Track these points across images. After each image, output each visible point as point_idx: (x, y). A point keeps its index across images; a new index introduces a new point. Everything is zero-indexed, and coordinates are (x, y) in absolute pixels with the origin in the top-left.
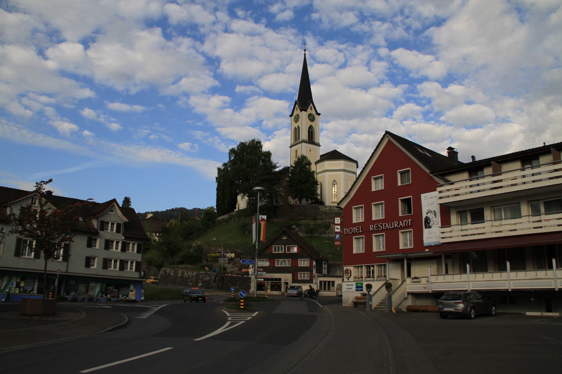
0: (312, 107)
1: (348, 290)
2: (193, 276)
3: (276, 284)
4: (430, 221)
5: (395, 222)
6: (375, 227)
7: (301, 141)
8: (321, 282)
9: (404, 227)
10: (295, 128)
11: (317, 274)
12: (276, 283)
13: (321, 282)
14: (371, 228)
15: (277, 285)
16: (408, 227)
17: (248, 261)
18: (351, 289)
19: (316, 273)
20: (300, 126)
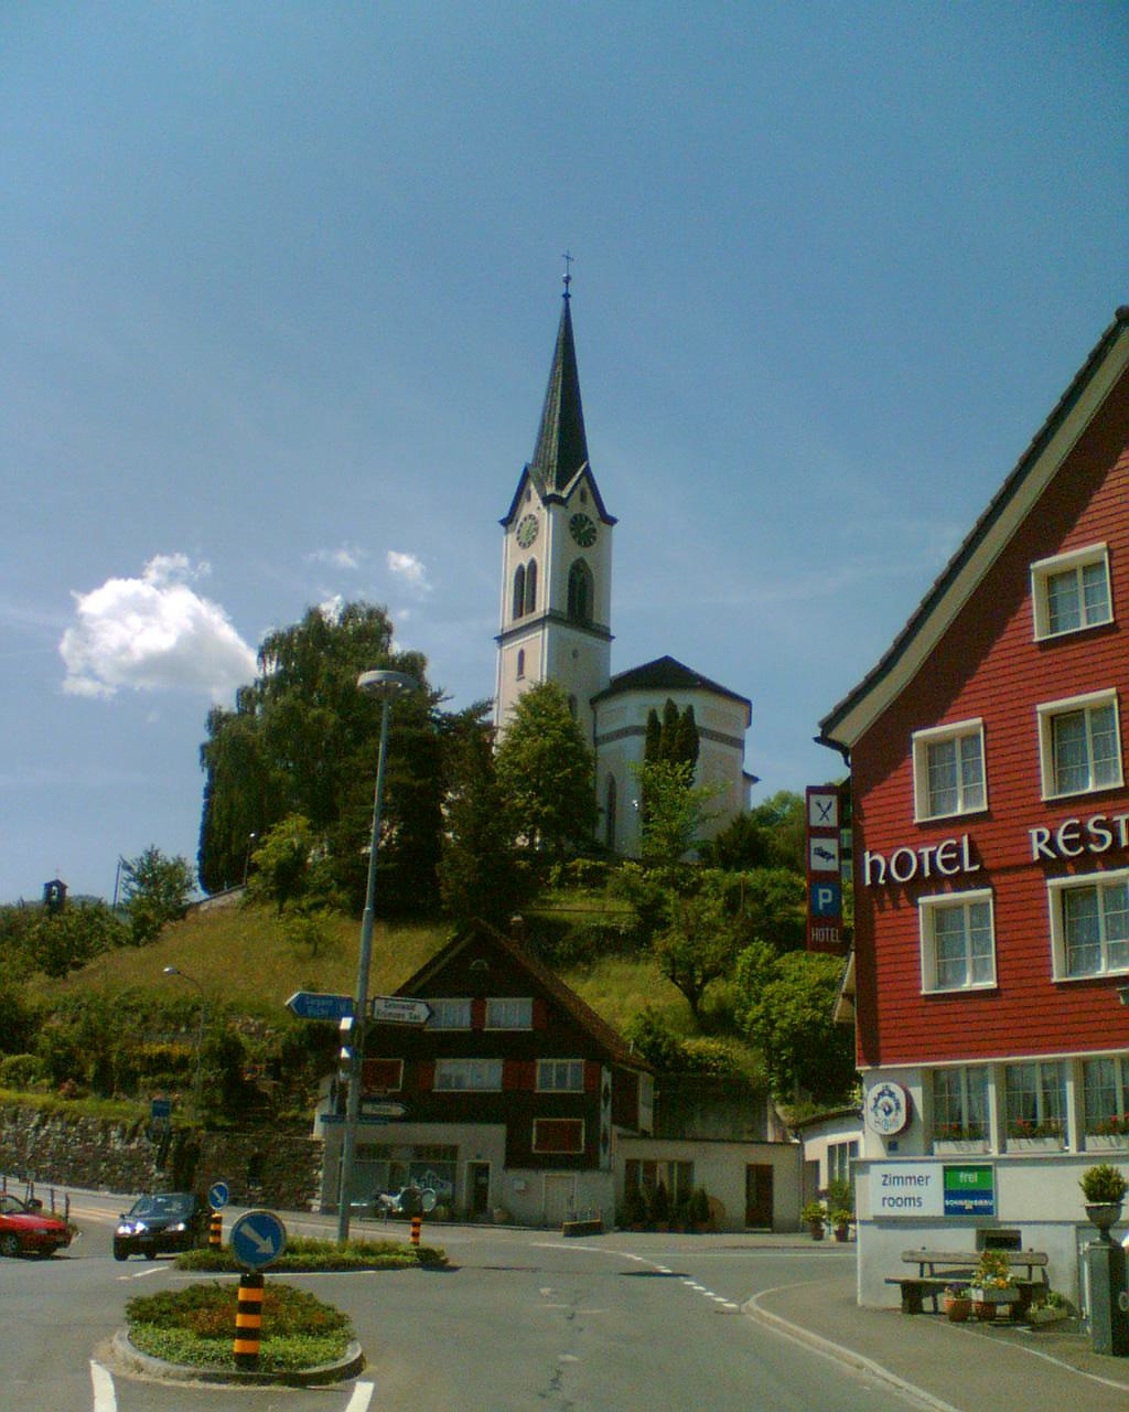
0: (588, 491)
6: (1060, 838)
7: (542, 616)
8: (631, 1165)
10: (521, 568)
11: (617, 1129)
13: (631, 1165)
14: (1037, 847)
18: (918, 1201)
19: (614, 1121)
20: (538, 562)
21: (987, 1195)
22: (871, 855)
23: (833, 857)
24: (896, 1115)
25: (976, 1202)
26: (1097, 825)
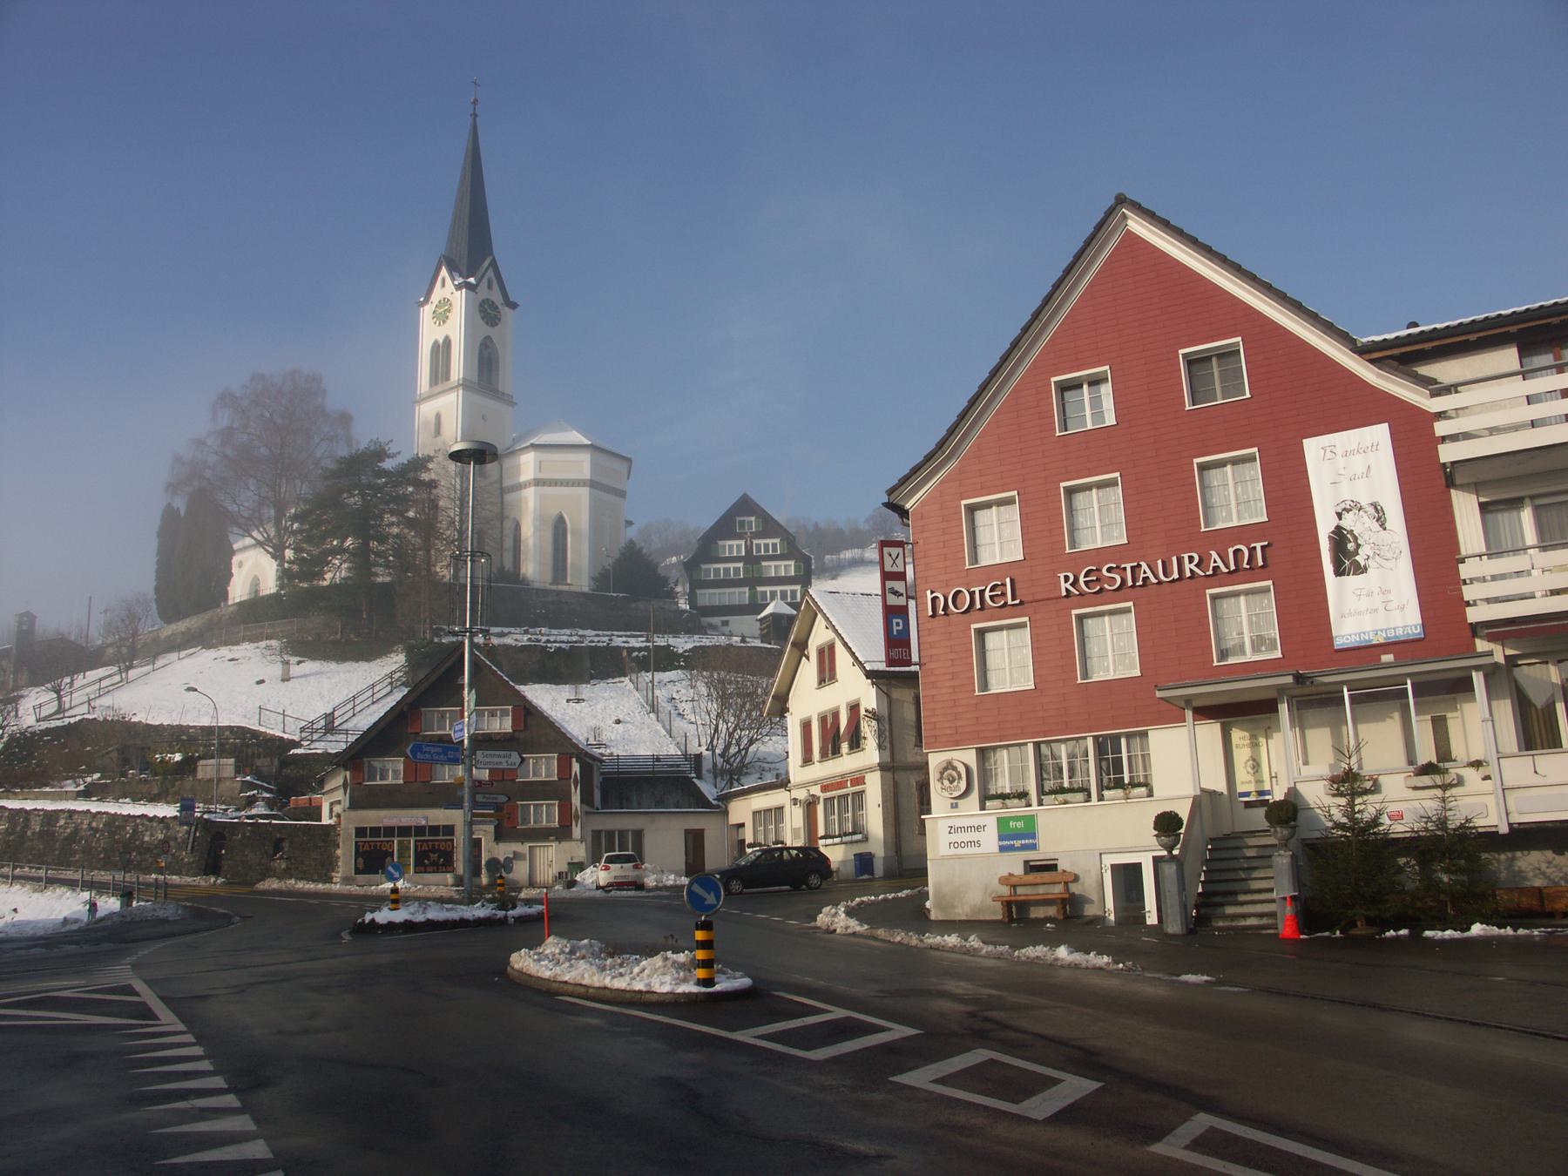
1: (960, 851)
2: (96, 830)
3: (433, 845)
4: (1358, 546)
5: (1186, 556)
6: (1082, 579)
9: (1230, 572)
10: (436, 342)
12: (378, 844)
15: (439, 850)
16: (1253, 572)
17: (437, 749)
18: (978, 843)
21: (1033, 836)
22: (932, 592)
23: (902, 595)
24: (959, 782)
25: (1023, 842)
26: (1109, 570)
